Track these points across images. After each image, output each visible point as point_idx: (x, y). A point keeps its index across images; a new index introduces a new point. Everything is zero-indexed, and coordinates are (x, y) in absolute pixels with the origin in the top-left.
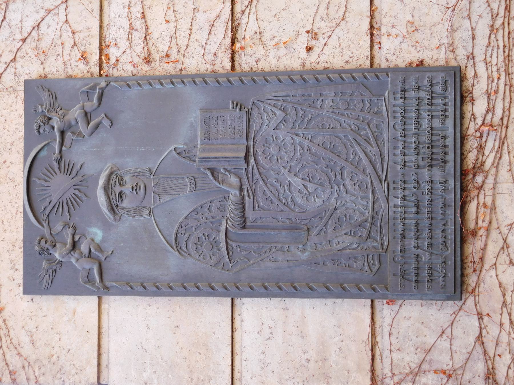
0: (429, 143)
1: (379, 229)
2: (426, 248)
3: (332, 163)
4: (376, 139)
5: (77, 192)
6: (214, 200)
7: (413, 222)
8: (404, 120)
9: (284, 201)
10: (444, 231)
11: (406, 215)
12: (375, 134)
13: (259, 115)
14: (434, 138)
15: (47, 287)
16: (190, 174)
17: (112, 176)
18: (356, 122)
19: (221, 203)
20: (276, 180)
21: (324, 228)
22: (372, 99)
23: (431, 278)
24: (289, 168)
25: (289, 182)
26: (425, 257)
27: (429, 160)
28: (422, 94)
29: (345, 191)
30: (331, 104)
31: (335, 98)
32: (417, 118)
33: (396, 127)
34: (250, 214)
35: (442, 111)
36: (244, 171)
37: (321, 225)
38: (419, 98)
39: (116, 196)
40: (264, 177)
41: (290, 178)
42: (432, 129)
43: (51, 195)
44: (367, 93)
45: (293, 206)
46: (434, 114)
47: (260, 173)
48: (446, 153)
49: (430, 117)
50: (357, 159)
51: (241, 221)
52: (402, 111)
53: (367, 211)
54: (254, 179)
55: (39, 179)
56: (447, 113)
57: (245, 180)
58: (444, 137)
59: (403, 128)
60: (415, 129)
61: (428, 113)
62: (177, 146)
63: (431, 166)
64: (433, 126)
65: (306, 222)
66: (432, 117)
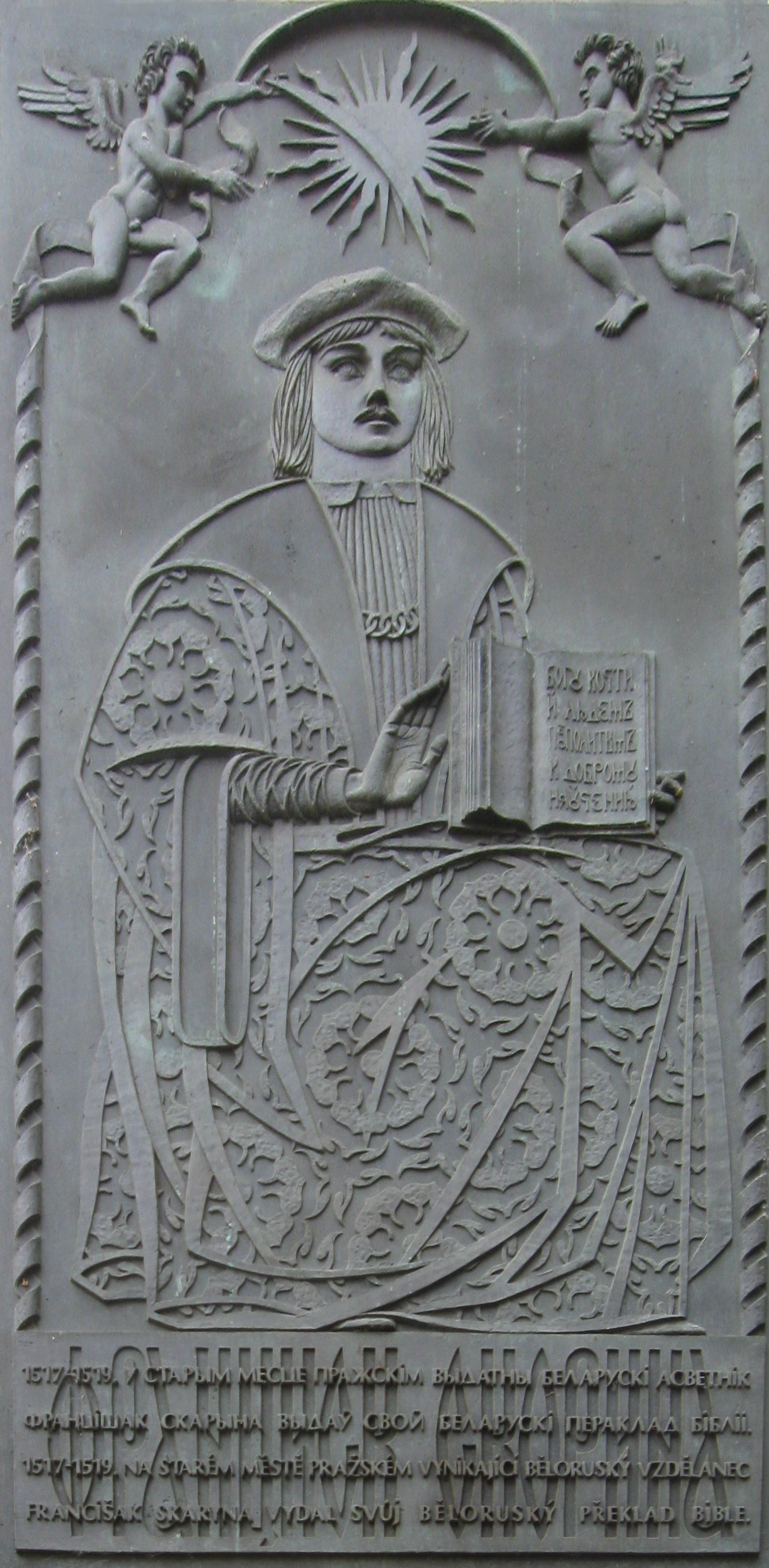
0: (521, 1469)
1: (232, 1298)
2: (168, 1454)
3: (462, 1140)
4: (540, 1290)
5: (367, 199)
6: (334, 709)
7: (256, 1416)
8: (604, 1387)
9: (328, 966)
10: (225, 1520)
11: (277, 1392)
12: (556, 1288)
13: (634, 877)
14: (540, 1488)
15: (28, 95)
16: (426, 620)
17: (423, 328)
18: (601, 1221)
19: (323, 733)
20: (401, 938)
21: (234, 1107)
22: (678, 1279)
23: (67, 1476)
24: (446, 983)
25: (397, 983)
26: (140, 1455)
27: (467, 1468)
28: (690, 1445)
29: (362, 1183)
30: (666, 1134)
31: (685, 1147)
32: (608, 1430)
33: (582, 1361)
34: (283, 840)
35: (630, 1512)
36: (436, 817)
37: (241, 1096)
38: (675, 1436)
39: (351, 337)
40: (411, 893)
41: (412, 990)
42: (570, 1479)
43: (356, 103)
44: (702, 1255)
45: (309, 996)
46: (622, 1488)
47: (426, 877)
48: (487, 1525)
49: (610, 1471)
50: (474, 1224)
51: (260, 801)
52: (635, 1378)
53: (292, 1259)
54: (409, 857)
55: (414, 58)
56: (621, 1530)
57: (402, 821)
58: (540, 1523)
59: (575, 1381)
60: (573, 1421)
61: (625, 1466)
62: (530, 573)
63: (445, 1477)
64: (579, 1483)
65: (256, 1044)
66: (611, 1480)
